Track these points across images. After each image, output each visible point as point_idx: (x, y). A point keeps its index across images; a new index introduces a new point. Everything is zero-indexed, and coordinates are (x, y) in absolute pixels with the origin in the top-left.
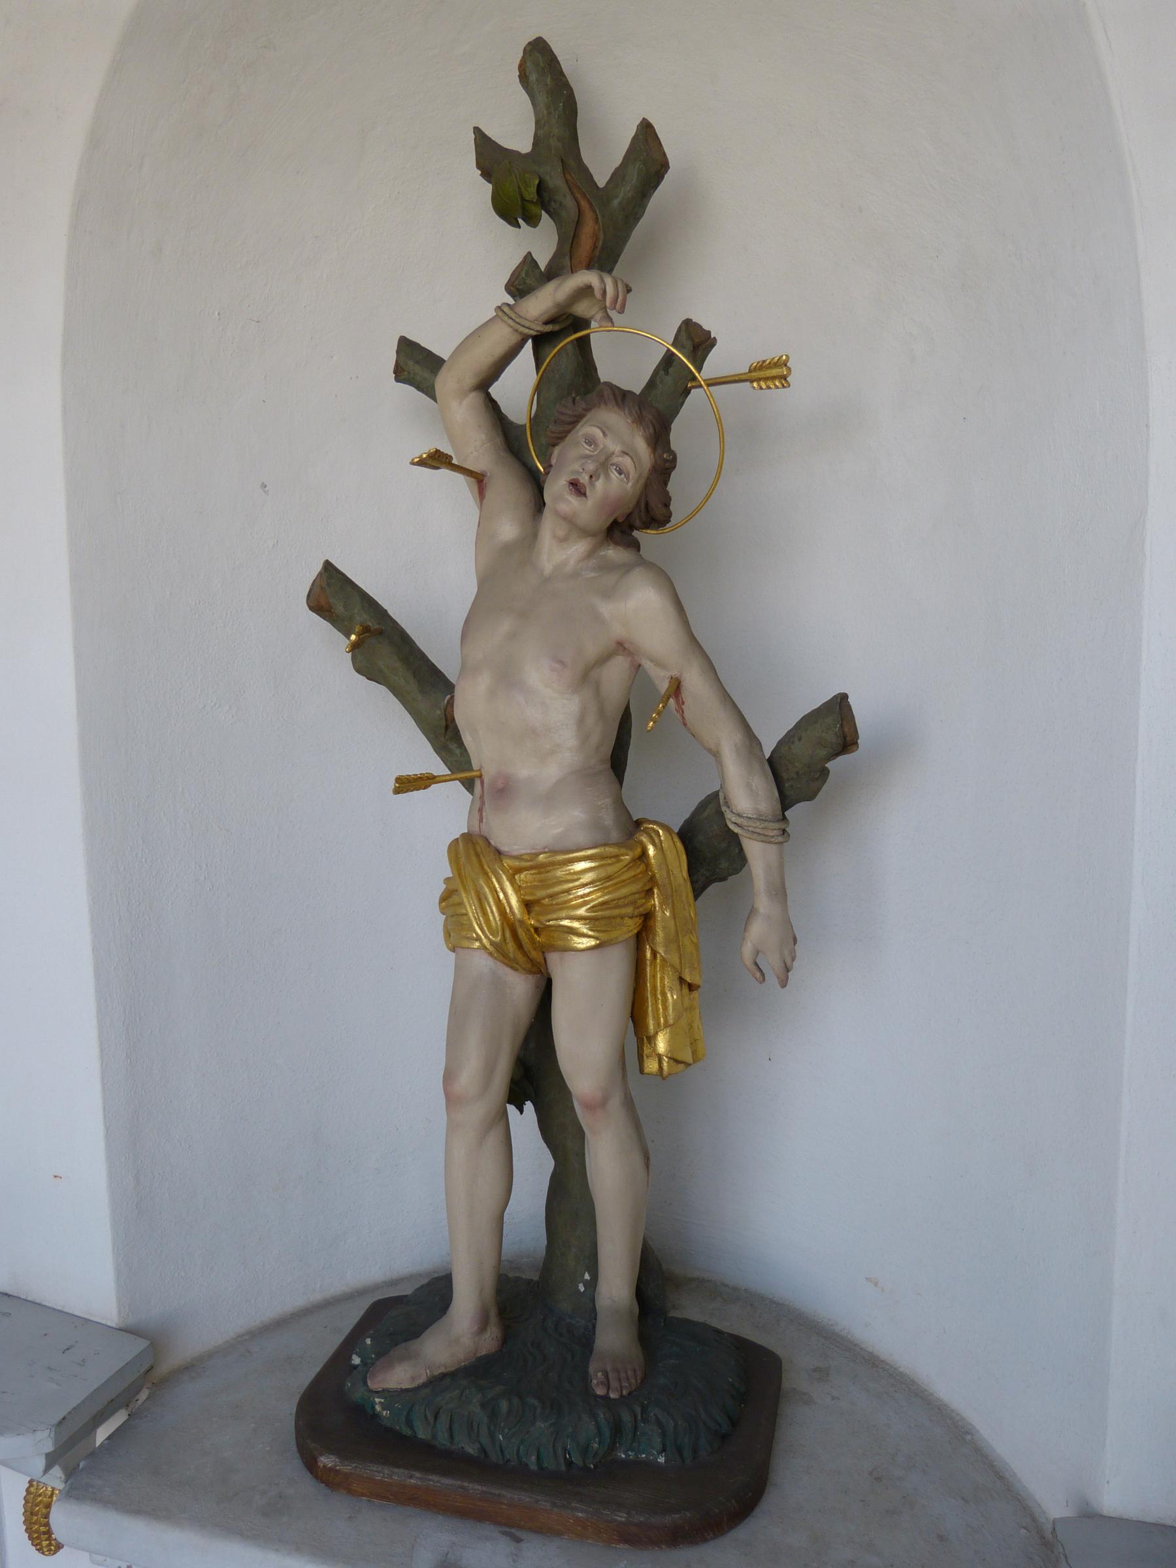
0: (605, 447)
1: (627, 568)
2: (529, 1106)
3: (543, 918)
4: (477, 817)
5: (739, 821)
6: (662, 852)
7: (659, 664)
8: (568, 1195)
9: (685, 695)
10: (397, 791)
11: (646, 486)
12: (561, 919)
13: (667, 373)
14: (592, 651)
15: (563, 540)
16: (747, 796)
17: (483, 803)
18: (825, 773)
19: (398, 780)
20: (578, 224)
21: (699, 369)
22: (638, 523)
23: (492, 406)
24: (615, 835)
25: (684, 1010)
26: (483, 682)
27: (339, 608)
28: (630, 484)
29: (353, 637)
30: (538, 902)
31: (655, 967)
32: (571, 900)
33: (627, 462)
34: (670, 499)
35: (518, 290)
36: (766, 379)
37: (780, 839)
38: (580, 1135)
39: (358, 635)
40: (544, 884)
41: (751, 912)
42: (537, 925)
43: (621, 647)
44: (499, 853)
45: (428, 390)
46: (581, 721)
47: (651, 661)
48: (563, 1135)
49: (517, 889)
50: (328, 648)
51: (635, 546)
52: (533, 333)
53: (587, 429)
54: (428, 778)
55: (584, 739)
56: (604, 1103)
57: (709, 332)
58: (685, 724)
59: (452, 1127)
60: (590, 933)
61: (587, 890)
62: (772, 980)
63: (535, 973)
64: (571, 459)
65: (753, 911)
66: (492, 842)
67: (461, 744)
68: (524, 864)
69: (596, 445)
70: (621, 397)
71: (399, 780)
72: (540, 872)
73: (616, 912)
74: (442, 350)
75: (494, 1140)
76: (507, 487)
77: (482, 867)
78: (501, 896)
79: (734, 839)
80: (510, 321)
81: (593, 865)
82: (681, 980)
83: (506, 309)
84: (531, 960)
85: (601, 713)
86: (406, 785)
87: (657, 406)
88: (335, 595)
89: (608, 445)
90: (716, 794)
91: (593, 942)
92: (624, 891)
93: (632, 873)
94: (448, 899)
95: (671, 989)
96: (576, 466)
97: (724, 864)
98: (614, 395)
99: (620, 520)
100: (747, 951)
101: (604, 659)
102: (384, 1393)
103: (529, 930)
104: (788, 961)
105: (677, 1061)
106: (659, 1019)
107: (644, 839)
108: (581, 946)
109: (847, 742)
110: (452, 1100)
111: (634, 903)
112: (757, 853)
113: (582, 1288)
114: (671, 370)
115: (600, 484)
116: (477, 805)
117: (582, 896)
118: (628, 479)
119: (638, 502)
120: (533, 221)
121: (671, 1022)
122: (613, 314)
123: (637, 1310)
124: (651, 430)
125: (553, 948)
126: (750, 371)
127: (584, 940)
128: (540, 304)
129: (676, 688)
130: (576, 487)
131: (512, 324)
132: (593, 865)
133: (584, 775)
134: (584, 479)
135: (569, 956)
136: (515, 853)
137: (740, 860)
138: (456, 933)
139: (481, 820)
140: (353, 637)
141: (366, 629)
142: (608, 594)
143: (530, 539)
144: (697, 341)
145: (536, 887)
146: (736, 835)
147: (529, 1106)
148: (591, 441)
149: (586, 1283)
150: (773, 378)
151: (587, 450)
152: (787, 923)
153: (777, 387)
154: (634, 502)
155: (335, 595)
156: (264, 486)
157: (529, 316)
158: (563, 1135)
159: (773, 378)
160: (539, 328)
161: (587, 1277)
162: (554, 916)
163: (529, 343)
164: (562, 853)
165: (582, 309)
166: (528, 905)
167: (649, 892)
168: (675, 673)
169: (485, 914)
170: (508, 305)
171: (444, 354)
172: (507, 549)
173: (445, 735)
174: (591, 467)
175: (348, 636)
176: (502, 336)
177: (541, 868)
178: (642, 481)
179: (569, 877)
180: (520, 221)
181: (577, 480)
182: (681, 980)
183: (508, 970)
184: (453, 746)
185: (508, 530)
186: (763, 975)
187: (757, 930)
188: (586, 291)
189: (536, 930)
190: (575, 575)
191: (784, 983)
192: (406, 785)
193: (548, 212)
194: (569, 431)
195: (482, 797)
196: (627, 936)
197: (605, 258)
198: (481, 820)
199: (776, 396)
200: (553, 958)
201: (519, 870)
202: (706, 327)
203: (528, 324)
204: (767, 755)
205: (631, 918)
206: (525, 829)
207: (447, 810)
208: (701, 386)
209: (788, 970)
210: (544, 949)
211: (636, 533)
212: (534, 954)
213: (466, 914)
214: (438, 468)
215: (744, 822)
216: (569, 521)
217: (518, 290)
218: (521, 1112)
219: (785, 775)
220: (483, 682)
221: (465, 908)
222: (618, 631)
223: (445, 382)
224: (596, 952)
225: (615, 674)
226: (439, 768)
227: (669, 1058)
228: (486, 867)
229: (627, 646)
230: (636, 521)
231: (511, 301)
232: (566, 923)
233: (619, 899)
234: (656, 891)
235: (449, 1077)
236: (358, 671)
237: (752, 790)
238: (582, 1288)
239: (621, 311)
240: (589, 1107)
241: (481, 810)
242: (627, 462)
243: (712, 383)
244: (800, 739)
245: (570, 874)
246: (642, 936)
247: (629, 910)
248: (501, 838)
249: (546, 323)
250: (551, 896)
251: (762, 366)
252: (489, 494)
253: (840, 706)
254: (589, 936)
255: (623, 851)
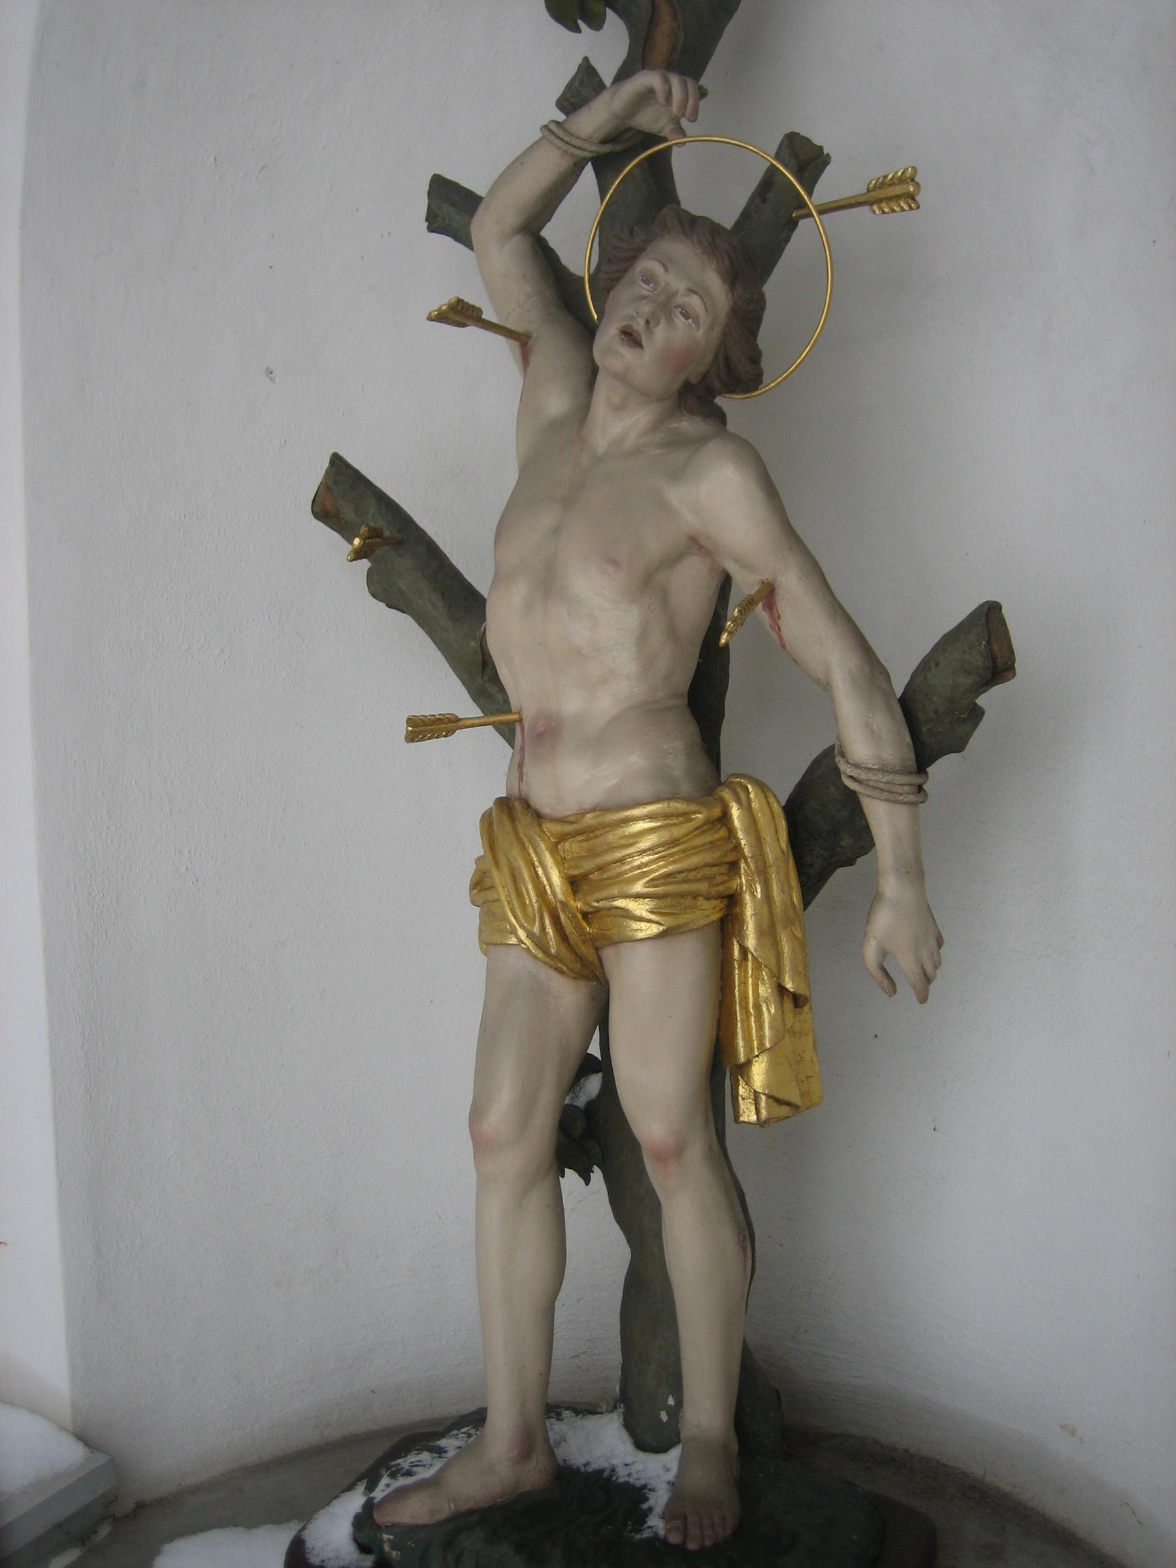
0: (667, 285)
1: (698, 442)
2: (597, 1175)
3: (590, 898)
4: (516, 774)
5: (855, 773)
6: (755, 820)
7: (745, 565)
8: (646, 1295)
9: (782, 605)
10: (412, 738)
11: (724, 334)
12: (614, 898)
13: (764, 201)
14: (655, 546)
15: (619, 408)
16: (867, 740)
17: (523, 758)
18: (976, 714)
19: (411, 721)
20: (653, 22)
21: (810, 194)
22: (717, 385)
23: (545, 258)
24: (686, 788)
25: (783, 1032)
26: (519, 591)
27: (348, 512)
28: (701, 332)
29: (357, 541)
30: (585, 876)
31: (746, 972)
32: (626, 872)
33: (695, 302)
34: (760, 354)
35: (571, 103)
36: (889, 199)
37: (912, 798)
38: (656, 1208)
39: (364, 538)
40: (593, 853)
41: (875, 898)
42: (586, 909)
43: (696, 544)
44: (539, 817)
45: (465, 239)
46: (642, 639)
47: (736, 561)
48: (636, 1211)
49: (561, 862)
50: (333, 565)
51: (720, 417)
52: (590, 155)
53: (647, 264)
54: (450, 721)
55: (647, 665)
56: (678, 1151)
57: (821, 148)
58: (784, 647)
59: (484, 1182)
60: (653, 917)
61: (646, 859)
62: (906, 993)
63: (587, 978)
64: (627, 305)
65: (876, 898)
66: (532, 804)
67: (502, 689)
68: (568, 828)
69: (656, 284)
70: (692, 225)
71: (411, 721)
72: (586, 837)
73: (684, 887)
74: (478, 185)
75: (537, 1201)
76: (552, 347)
77: (517, 834)
78: (540, 871)
79: (852, 799)
80: (557, 141)
81: (653, 824)
82: (781, 990)
83: (553, 127)
84: (580, 958)
85: (672, 632)
86: (424, 728)
87: (752, 248)
88: (347, 499)
89: (681, 290)
90: (832, 748)
91: (655, 929)
92: (694, 860)
93: (707, 838)
94: (480, 884)
95: (766, 1001)
96: (630, 310)
97: (846, 841)
98: (681, 223)
99: (693, 381)
100: (871, 952)
101: (672, 560)
102: (391, 1528)
103: (575, 916)
104: (929, 968)
105: (779, 1101)
106: (751, 1041)
107: (726, 794)
108: (641, 935)
109: (998, 666)
110: (481, 1145)
111: (710, 879)
112: (884, 819)
113: (664, 1417)
114: (770, 195)
115: (660, 332)
116: (517, 759)
117: (639, 867)
118: (697, 322)
119: (716, 357)
120: (596, 23)
121: (768, 1045)
122: (684, 122)
123: (735, 1447)
124: (727, 261)
125: (613, 943)
126: (869, 191)
127: (643, 925)
128: (594, 120)
129: (768, 594)
130: (630, 337)
131: (560, 144)
132: (653, 824)
133: (648, 711)
134: (639, 325)
135: (625, 948)
136: (559, 815)
137: (864, 841)
138: (492, 936)
139: (521, 779)
140: (357, 541)
141: (375, 533)
142: (676, 475)
143: (583, 411)
144: (807, 159)
145: (581, 858)
146: (853, 795)
147: (597, 1175)
148: (649, 279)
149: (669, 1410)
150: (898, 197)
151: (645, 289)
152: (926, 914)
153: (894, 211)
154: (708, 359)
155: (347, 499)
156: (270, 372)
157: (582, 135)
158: (636, 1211)
159: (898, 197)
160: (594, 148)
161: (671, 1401)
162: (604, 894)
163: (589, 172)
164: (612, 809)
165: (647, 120)
166: (575, 883)
167: (733, 867)
168: (767, 576)
169: (523, 905)
170: (557, 123)
171: (480, 190)
172: (555, 426)
173: (481, 675)
174: (646, 309)
175: (351, 542)
176: (550, 164)
177: (588, 832)
178: (718, 329)
179: (623, 842)
180: (580, 22)
181: (629, 326)
182: (781, 990)
183: (554, 975)
184: (493, 690)
185: (557, 402)
186: (893, 984)
187: (883, 921)
188: (648, 95)
189: (585, 915)
190: (636, 452)
191: (923, 998)
192: (424, 728)
193: (616, 11)
194: (625, 271)
195: (522, 749)
196: (706, 921)
197: (690, 60)
198: (521, 779)
199: (900, 220)
200: (608, 954)
201: (563, 838)
202: (817, 141)
203: (579, 143)
204: (899, 691)
205: (708, 898)
206: (572, 782)
207: (478, 766)
208: (811, 215)
209: (928, 979)
210: (600, 943)
211: (719, 401)
212: (586, 951)
213: (498, 900)
214: (464, 325)
215: (863, 776)
216: (622, 378)
217: (571, 103)
218: (587, 1183)
219: (921, 716)
220: (519, 591)
221: (498, 893)
222: (689, 520)
223: (484, 225)
224: (659, 942)
225: (690, 589)
226: (467, 708)
227: (769, 1096)
228: (522, 835)
229: (702, 542)
230: (715, 386)
231: (560, 117)
232: (620, 903)
233: (690, 870)
234: (743, 865)
235: (477, 1113)
236: (375, 596)
237: (872, 733)
238: (664, 1417)
239: (693, 118)
240: (661, 1158)
241: (521, 766)
242: (695, 302)
243: (823, 210)
244: (937, 664)
245: (626, 837)
246: (727, 925)
247: (703, 887)
248: (543, 797)
249: (604, 142)
250: (601, 868)
251: (883, 184)
252: (534, 359)
253: (989, 618)
254: (649, 921)
255: (693, 807)
